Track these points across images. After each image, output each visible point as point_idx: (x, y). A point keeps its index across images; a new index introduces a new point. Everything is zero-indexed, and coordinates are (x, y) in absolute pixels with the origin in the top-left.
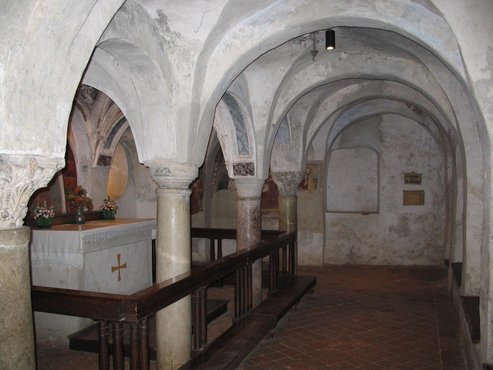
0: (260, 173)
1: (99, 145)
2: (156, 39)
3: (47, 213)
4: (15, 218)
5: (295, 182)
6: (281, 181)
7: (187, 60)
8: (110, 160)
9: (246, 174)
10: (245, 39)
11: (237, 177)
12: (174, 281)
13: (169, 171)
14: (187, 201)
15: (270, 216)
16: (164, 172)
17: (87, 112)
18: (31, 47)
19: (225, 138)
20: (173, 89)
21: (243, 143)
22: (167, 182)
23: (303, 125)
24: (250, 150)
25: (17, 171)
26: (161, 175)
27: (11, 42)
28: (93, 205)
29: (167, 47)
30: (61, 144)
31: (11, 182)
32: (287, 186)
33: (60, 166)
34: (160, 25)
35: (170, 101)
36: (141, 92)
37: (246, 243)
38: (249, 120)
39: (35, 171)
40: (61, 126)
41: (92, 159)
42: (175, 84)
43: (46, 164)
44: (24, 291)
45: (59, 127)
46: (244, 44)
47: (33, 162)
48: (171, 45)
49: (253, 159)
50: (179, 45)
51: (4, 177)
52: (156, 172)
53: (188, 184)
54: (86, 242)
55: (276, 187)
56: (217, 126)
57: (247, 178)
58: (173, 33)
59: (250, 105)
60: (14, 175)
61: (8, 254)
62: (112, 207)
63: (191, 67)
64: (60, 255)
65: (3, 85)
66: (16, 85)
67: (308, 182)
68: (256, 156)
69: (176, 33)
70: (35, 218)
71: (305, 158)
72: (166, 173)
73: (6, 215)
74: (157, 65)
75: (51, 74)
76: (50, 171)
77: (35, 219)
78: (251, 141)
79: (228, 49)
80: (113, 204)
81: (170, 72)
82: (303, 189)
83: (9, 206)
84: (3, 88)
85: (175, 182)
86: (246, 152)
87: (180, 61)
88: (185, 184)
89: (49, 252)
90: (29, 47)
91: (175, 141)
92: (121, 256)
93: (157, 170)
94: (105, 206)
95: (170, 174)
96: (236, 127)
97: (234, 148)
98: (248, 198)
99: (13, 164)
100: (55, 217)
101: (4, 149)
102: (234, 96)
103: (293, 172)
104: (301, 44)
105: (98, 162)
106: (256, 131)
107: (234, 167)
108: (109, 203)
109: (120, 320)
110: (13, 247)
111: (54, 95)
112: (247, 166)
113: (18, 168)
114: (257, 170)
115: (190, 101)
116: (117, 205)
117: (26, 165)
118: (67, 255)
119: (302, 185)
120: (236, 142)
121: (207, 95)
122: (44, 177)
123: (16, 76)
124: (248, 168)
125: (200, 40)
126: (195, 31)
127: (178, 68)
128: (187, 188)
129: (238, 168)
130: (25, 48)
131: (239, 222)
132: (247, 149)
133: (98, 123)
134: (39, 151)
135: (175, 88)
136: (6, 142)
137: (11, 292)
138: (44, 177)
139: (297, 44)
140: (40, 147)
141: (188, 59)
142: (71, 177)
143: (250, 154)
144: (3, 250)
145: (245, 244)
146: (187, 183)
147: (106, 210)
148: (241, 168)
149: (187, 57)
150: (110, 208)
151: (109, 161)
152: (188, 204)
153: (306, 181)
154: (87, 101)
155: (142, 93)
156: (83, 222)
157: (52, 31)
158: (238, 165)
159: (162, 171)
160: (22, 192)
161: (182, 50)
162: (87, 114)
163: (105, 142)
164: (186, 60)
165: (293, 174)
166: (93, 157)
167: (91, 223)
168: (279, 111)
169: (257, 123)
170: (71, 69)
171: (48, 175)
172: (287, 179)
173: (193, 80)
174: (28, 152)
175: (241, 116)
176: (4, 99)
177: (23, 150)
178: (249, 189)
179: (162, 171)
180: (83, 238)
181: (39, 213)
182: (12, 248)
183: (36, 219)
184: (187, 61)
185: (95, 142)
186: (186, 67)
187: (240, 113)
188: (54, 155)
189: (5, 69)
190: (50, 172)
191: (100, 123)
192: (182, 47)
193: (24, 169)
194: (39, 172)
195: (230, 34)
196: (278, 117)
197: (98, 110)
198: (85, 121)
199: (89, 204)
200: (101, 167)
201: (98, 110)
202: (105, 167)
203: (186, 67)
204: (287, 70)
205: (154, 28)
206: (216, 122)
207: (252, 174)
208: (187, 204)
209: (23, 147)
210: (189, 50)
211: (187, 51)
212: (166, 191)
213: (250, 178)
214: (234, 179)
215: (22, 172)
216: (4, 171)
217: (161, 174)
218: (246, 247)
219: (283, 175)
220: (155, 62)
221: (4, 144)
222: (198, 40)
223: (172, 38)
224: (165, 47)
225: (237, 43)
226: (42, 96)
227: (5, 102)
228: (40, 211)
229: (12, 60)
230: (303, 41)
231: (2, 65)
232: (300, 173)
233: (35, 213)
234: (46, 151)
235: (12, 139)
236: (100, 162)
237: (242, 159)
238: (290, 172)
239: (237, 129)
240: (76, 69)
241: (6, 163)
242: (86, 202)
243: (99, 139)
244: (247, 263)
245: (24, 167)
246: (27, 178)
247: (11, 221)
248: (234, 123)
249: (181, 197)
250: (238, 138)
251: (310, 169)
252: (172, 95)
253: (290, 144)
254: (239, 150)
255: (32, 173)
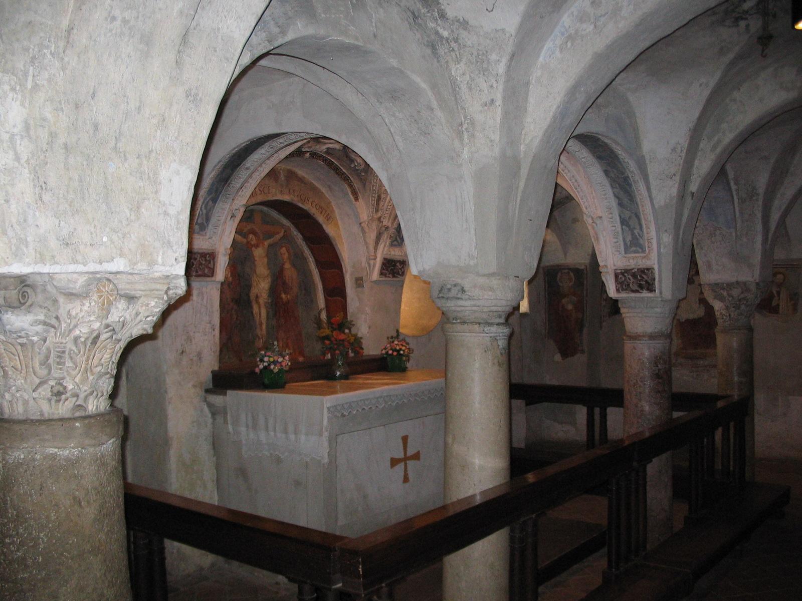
0: (666, 285)
1: (381, 241)
2: (418, 36)
3: (278, 362)
4: (82, 396)
5: (747, 302)
6: (721, 299)
7: (485, 71)
8: (403, 267)
9: (639, 289)
10: (602, 19)
11: (623, 295)
12: (478, 500)
13: (463, 291)
14: (501, 347)
15: (706, 363)
16: (454, 292)
17: (357, 185)
18: (79, 57)
19: (598, 222)
20: (463, 130)
21: (632, 230)
22: (462, 311)
23: (761, 191)
24: (647, 244)
25: (69, 306)
26: (448, 298)
27: (31, 50)
28: (364, 348)
29: (446, 51)
30: (174, 248)
31: (58, 327)
32: (733, 309)
33: (174, 291)
34: (427, 8)
35: (458, 156)
36: (403, 141)
37: (640, 420)
38: (642, 186)
39: (110, 303)
40: (172, 211)
41: (369, 266)
42: (466, 122)
43: (143, 288)
44: (101, 537)
45: (166, 213)
46: (601, 31)
47: (104, 287)
48: (453, 45)
49: (652, 261)
50: (469, 43)
51: (41, 317)
52: (440, 291)
53: (503, 313)
54: (336, 416)
55: (712, 307)
56: (582, 199)
57: (642, 298)
58: (453, 21)
59: (643, 157)
60: (62, 312)
61: (65, 465)
62: (401, 349)
63: (495, 85)
64: (292, 437)
65: (22, 138)
66: (53, 135)
67: (779, 299)
68: (658, 254)
69: (458, 21)
70: (257, 370)
71: (767, 254)
72: (457, 295)
73: (61, 389)
74: (423, 85)
75: (139, 108)
76: (152, 302)
77: (257, 373)
78: (648, 228)
79: (569, 44)
80: (404, 344)
81: (456, 99)
82: (770, 312)
83: (65, 374)
84: (22, 143)
85: (475, 311)
86: (638, 249)
87: (472, 75)
88: (495, 314)
89: (275, 430)
90: (76, 58)
91: (473, 232)
92: (409, 440)
93: (441, 289)
94: (389, 348)
95: (464, 297)
96: (617, 201)
97: (616, 240)
98: (644, 336)
99: (61, 293)
100: (291, 369)
101: (36, 263)
102: (606, 141)
103: (745, 283)
104: (738, 26)
105: (381, 270)
106: (656, 207)
107: (616, 276)
108: (396, 342)
109: (334, 587)
110: (76, 453)
111: (152, 150)
112: (640, 273)
113: (70, 300)
114: (660, 281)
115: (497, 151)
116: (411, 346)
117: (90, 293)
118: (303, 437)
119: (767, 305)
120: (620, 229)
121: (532, 140)
122: (137, 314)
123: (49, 116)
124: (643, 277)
125: (507, 29)
126: (487, 10)
127: (470, 89)
128: (502, 321)
129: (623, 279)
130: (66, 59)
131: (628, 381)
132: (641, 241)
133: (378, 204)
134: (119, 265)
135: (466, 129)
136: (38, 250)
137: (73, 540)
138: (137, 314)
139: (729, 27)
140: (121, 255)
141: (487, 69)
142: (338, 298)
143: (647, 251)
144: (55, 459)
145: (638, 422)
146: (500, 313)
147: (390, 354)
148: (629, 278)
149: (485, 66)
150: (398, 351)
151: (401, 269)
152: (504, 352)
153: (776, 298)
154: (356, 166)
155: (405, 141)
156: (345, 377)
157: (125, 22)
158: (624, 273)
159: (449, 290)
160: (88, 346)
161: (475, 53)
162: (359, 189)
163: (392, 235)
164: (484, 71)
165: (744, 286)
166: (372, 262)
167: (361, 379)
168: (704, 166)
169: (659, 192)
170: (187, 96)
171: (148, 310)
172: (732, 297)
173: (499, 111)
174: (92, 267)
175: (626, 179)
176: (25, 165)
177: (80, 263)
178: (646, 319)
179: (449, 290)
180: (329, 409)
181: (264, 362)
182: (73, 455)
183: (259, 373)
184: (485, 74)
185: (372, 236)
186: (484, 86)
187: (623, 173)
188: (160, 270)
189: (22, 105)
190: (152, 305)
191: (381, 204)
192: (473, 47)
193: (84, 302)
194: (122, 304)
195: (572, 13)
196: (700, 176)
197: (375, 181)
198: (356, 200)
199: (357, 343)
200: (387, 279)
201: (375, 181)
202: (394, 279)
203: (484, 86)
204: (712, 83)
205: (413, 13)
206: (581, 193)
207: (651, 289)
208: (501, 354)
209: (79, 258)
210: (487, 52)
211: (483, 53)
212: (459, 327)
213: (647, 297)
214: (617, 299)
215: (79, 306)
216: (41, 307)
217: (448, 295)
218: (641, 429)
219: (723, 289)
220: (417, 79)
221: (34, 253)
222: (503, 30)
223: (452, 31)
224: (441, 51)
225: (588, 30)
226: (122, 155)
227: (29, 170)
228: (266, 359)
229: (37, 85)
230: (742, 19)
231: (15, 96)
232: (757, 284)
233: (257, 362)
234: (135, 264)
235: (53, 243)
236: (384, 271)
237: (631, 261)
238: (737, 282)
239: (620, 204)
240: (200, 95)
241: (45, 290)
242: (350, 343)
243: (382, 232)
244: (635, 464)
245: (85, 298)
246: (92, 318)
247: (74, 402)
248: (614, 193)
249: (488, 339)
250: (623, 222)
251: (783, 275)
252: (462, 144)
253: (736, 228)
254: (625, 244)
255: (106, 308)
